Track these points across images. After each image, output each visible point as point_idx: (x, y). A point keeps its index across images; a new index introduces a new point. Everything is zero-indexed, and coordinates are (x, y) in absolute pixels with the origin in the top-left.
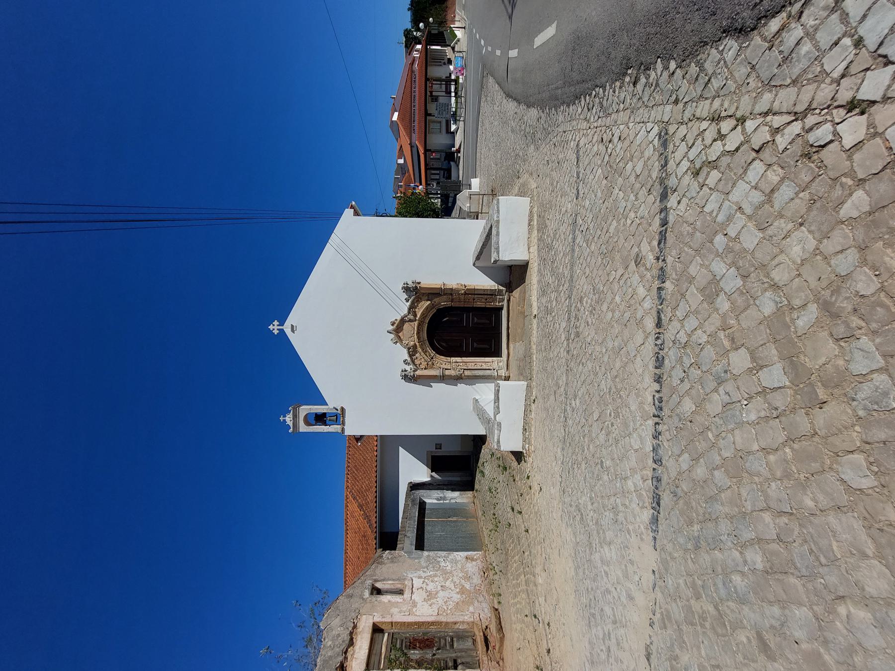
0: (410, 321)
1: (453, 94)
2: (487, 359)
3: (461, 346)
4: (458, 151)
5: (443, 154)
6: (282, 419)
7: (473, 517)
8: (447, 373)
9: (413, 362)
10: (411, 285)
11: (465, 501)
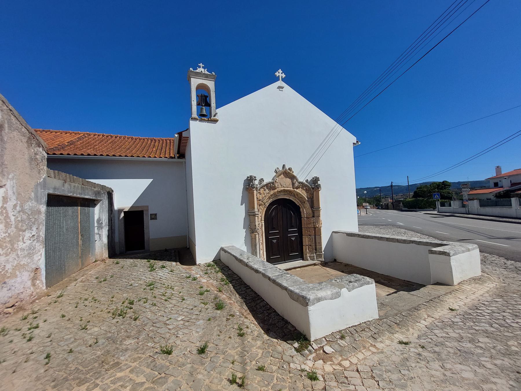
0: (293, 184)
3: (274, 229)
7: (83, 264)
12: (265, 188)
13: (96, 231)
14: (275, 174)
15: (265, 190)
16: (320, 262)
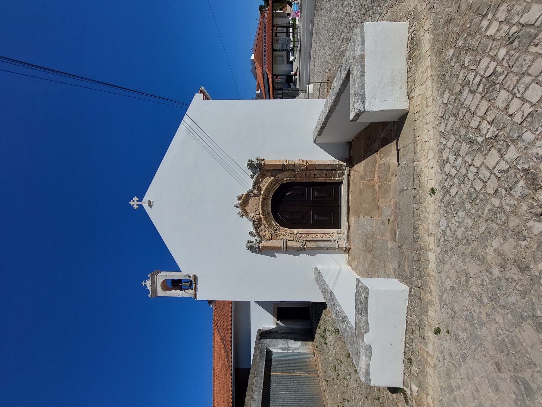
0: (255, 195)
1: (291, 34)
2: (327, 231)
3: (303, 218)
4: (296, 74)
5: (285, 78)
6: (143, 283)
8: (290, 244)
10: (255, 161)
11: (306, 351)
12: (259, 229)
13: (291, 351)
14: (244, 217)
15: (262, 230)
16: (347, 168)
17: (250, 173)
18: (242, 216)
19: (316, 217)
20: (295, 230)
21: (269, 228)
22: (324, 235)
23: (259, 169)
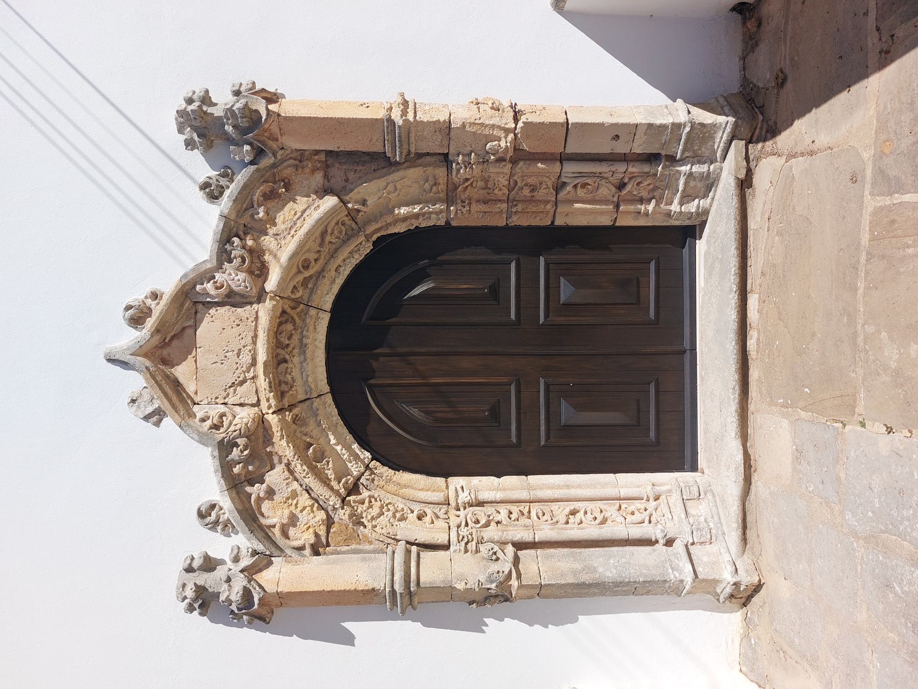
0: (233, 299)
3: (496, 414)
8: (433, 570)
9: (251, 517)
12: (256, 490)
14: (168, 422)
15: (271, 493)
17: (201, 168)
18: (156, 417)
19: (567, 413)
20: (457, 482)
21: (311, 481)
22: (611, 510)
23: (251, 146)
